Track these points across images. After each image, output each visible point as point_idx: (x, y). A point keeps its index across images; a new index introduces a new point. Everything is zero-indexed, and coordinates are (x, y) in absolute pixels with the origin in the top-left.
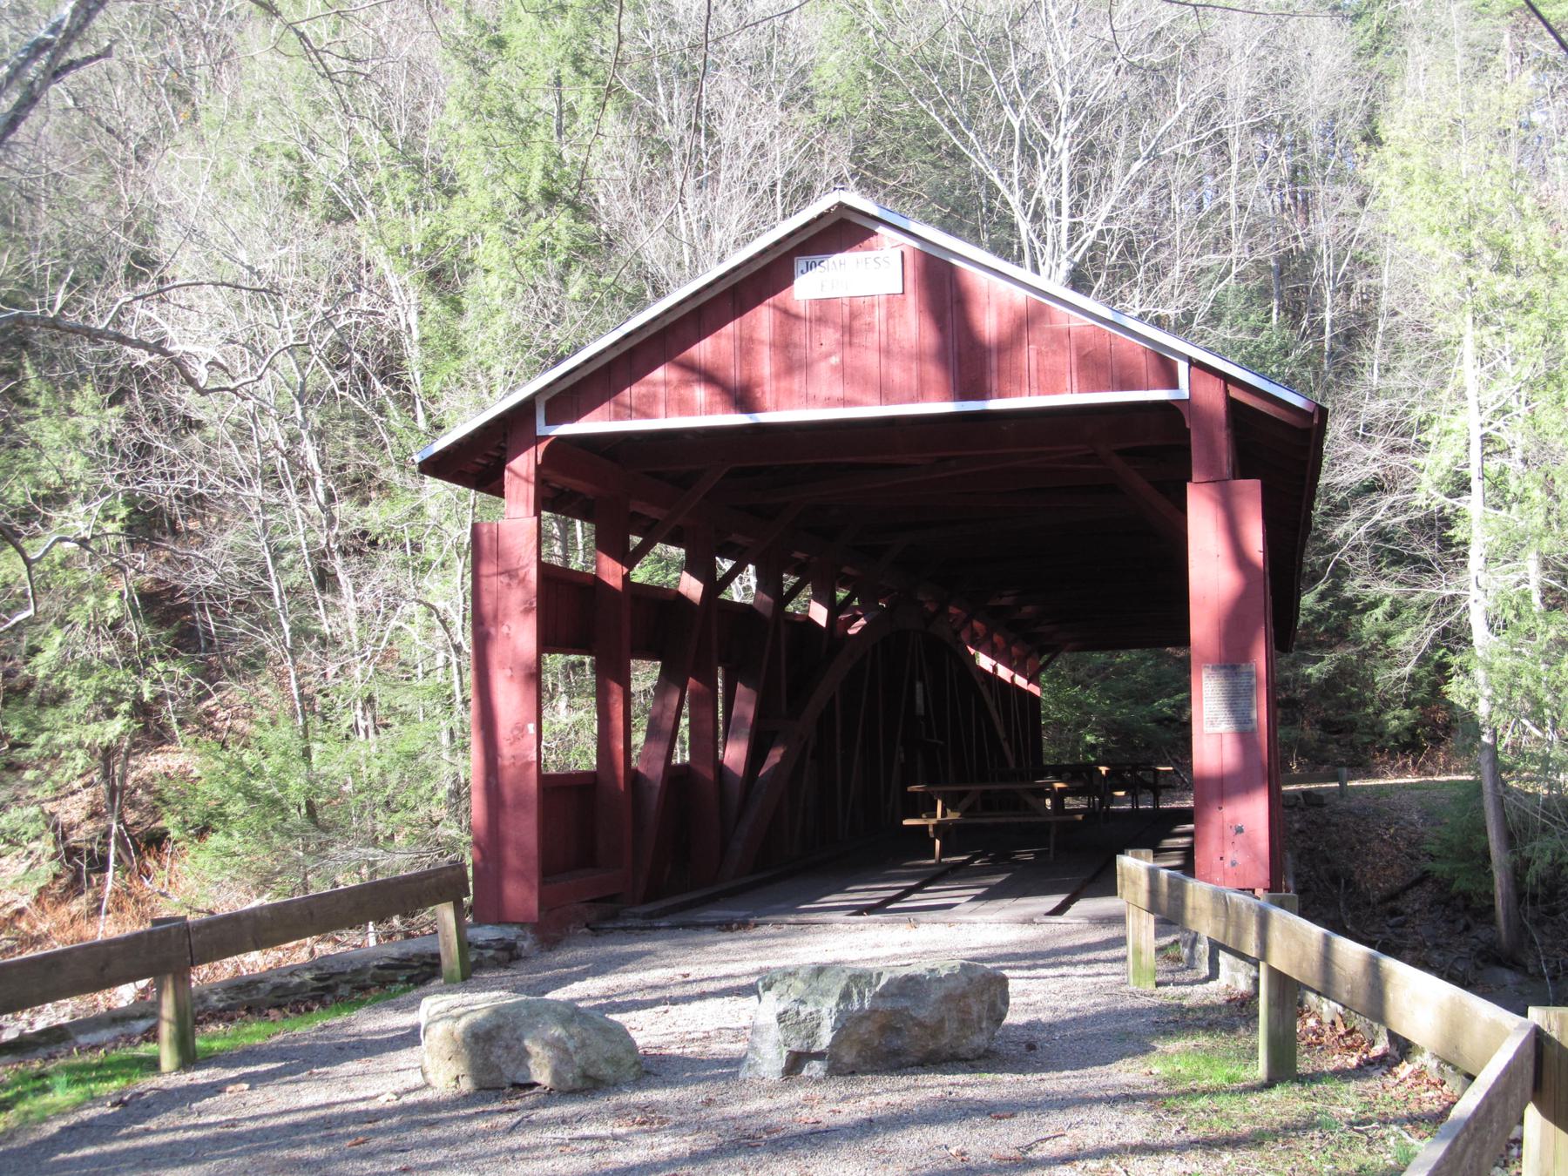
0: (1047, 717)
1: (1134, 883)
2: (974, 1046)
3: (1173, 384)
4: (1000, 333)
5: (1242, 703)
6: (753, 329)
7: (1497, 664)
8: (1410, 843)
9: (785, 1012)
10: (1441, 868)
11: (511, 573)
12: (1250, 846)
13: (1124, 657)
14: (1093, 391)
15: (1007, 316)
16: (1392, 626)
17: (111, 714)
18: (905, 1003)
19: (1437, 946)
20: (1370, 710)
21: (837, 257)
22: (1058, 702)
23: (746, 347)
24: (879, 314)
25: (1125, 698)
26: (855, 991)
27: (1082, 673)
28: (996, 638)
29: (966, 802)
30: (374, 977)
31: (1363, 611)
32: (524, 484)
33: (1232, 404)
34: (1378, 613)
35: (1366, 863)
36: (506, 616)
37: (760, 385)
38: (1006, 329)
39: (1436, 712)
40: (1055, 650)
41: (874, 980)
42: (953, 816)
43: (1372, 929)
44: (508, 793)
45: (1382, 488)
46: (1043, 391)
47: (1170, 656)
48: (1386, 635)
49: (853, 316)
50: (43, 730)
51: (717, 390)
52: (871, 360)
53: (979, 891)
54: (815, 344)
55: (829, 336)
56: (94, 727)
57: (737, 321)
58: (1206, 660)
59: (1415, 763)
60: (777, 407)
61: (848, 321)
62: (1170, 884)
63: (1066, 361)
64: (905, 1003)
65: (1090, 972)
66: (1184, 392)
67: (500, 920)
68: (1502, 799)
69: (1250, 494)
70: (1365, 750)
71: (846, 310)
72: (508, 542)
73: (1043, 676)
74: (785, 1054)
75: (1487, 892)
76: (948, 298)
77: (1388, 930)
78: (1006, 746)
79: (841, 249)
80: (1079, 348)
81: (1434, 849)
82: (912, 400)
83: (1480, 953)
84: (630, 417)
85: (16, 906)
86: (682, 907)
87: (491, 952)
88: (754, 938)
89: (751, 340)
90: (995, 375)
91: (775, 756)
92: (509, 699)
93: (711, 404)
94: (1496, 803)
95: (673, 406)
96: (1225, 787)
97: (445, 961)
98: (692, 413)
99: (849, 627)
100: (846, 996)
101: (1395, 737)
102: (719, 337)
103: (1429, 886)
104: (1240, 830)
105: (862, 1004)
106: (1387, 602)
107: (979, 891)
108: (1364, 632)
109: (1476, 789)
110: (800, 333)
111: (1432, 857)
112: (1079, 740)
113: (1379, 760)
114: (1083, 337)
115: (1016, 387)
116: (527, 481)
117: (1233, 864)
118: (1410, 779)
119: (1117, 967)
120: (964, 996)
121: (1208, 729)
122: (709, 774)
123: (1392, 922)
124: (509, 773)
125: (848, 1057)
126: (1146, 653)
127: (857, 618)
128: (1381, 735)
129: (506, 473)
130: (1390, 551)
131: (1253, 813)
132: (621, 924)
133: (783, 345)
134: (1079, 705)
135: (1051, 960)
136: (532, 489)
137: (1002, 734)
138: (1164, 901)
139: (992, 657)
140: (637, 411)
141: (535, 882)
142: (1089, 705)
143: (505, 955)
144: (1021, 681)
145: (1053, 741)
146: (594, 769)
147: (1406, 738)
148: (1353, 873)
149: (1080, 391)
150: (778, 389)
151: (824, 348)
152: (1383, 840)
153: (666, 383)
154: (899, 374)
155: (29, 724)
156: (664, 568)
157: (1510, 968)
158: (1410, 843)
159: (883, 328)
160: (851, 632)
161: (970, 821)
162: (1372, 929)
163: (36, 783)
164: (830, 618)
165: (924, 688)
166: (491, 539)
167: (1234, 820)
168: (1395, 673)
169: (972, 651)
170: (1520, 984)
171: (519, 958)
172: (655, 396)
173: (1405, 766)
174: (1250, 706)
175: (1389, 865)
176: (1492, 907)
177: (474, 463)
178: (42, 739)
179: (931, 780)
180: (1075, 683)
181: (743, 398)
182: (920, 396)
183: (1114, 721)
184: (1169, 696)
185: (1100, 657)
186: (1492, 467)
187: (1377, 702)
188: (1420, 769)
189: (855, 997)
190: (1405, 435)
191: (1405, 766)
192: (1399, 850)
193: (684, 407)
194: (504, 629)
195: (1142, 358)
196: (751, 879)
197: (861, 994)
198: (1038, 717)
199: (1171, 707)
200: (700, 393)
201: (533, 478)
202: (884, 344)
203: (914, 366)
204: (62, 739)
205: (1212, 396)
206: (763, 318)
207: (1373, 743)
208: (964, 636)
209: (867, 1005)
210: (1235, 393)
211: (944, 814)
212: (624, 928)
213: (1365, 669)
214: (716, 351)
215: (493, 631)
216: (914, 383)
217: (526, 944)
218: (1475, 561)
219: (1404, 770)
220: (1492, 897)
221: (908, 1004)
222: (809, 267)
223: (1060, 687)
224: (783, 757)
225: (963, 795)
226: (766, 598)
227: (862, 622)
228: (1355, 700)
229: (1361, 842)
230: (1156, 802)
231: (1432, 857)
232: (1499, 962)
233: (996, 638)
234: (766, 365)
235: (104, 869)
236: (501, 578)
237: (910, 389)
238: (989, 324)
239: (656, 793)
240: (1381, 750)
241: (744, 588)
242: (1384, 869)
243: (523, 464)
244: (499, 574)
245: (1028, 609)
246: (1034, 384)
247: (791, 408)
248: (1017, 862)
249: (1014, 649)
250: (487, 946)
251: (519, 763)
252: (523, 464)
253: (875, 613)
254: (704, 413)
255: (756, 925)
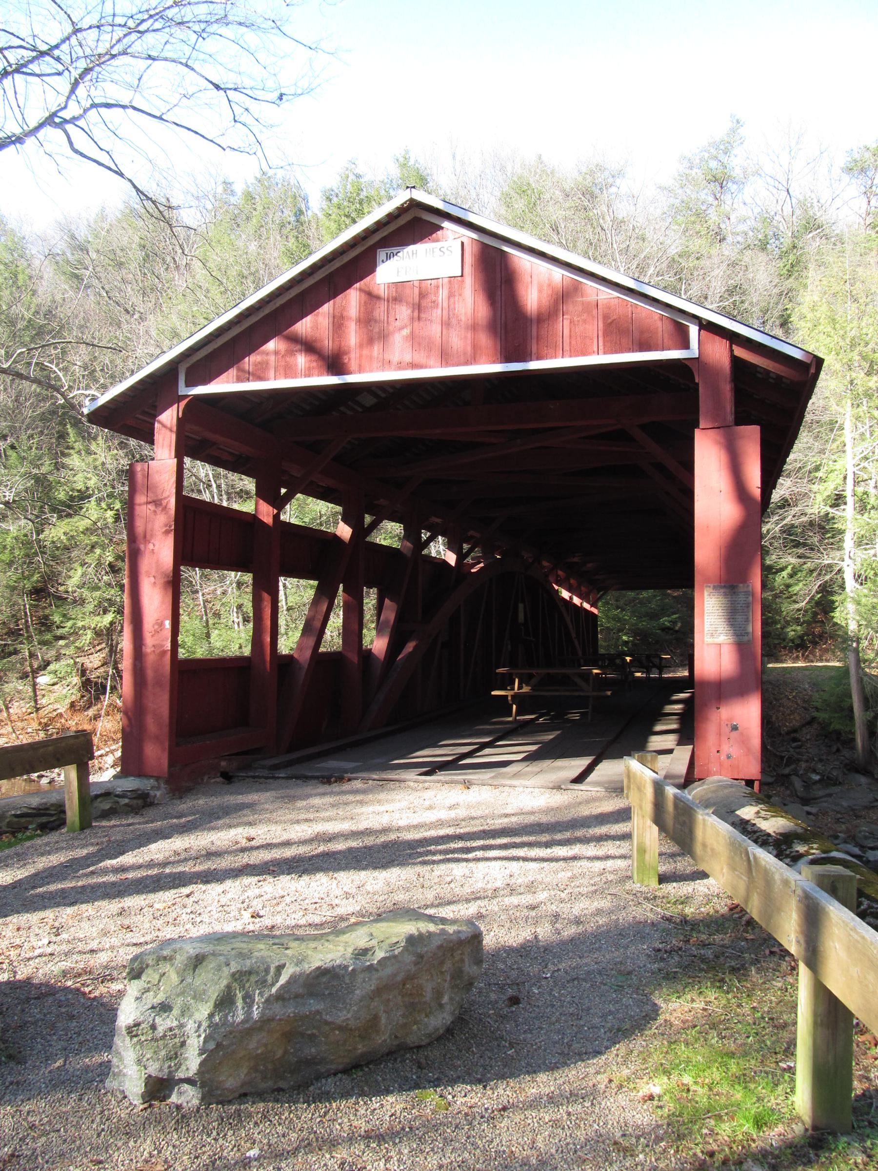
0: (602, 625)
1: (639, 789)
2: (431, 1028)
3: (685, 344)
4: (539, 307)
5: (740, 618)
6: (344, 308)
7: (864, 600)
8: (804, 701)
9: (137, 1025)
10: (823, 716)
11: (157, 503)
12: (744, 741)
13: (645, 594)
14: (616, 352)
15: (546, 292)
16: (791, 581)
17: (105, 611)
18: (314, 1005)
19: (821, 760)
20: (779, 626)
21: (411, 248)
22: (608, 617)
23: (338, 323)
24: (443, 294)
25: (645, 616)
26: (239, 995)
27: (621, 603)
28: (572, 581)
29: (534, 681)
30: (9, 824)
31: (776, 573)
32: (168, 433)
33: (736, 362)
34: (784, 574)
35: (779, 711)
36: (152, 535)
37: (347, 353)
38: (546, 302)
39: (814, 628)
40: (606, 589)
41: (269, 979)
42: (526, 689)
43: (782, 749)
44: (150, 674)
45: (789, 505)
46: (574, 353)
47: (669, 595)
48: (788, 586)
49: (422, 295)
50: (70, 619)
51: (314, 357)
52: (435, 330)
53: (534, 748)
54: (391, 319)
55: (403, 312)
56: (98, 618)
57: (331, 302)
58: (707, 581)
59: (803, 655)
60: (360, 370)
61: (419, 298)
62: (676, 806)
63: (594, 328)
64: (314, 1005)
65: (601, 852)
66: (694, 351)
67: (140, 773)
68: (862, 679)
69: (751, 440)
70: (775, 647)
71: (417, 291)
72: (156, 478)
73: (600, 604)
74: (144, 1077)
75: (850, 731)
76: (498, 276)
77: (791, 750)
78: (576, 642)
79: (414, 242)
80: (605, 317)
81: (818, 705)
82: (467, 363)
83: (846, 765)
84: (248, 380)
85: (59, 711)
86: (299, 761)
87: (126, 801)
88: (338, 794)
89: (342, 317)
90: (534, 341)
91: (410, 647)
92: (154, 601)
93: (309, 369)
94: (858, 681)
95: (281, 371)
96: (724, 690)
97: (69, 814)
98: (294, 376)
99: (473, 568)
100: (225, 1002)
101: (792, 641)
102: (317, 315)
103: (815, 726)
104: (735, 728)
105: (248, 1013)
106: (790, 568)
107: (534, 748)
108: (776, 584)
109: (844, 672)
110: (380, 311)
111: (817, 709)
112: (619, 638)
113: (783, 653)
114: (609, 308)
115: (551, 351)
116: (171, 431)
117: (729, 757)
118: (800, 664)
119: (622, 848)
120: (410, 977)
121: (708, 639)
122: (354, 658)
123: (794, 745)
124: (151, 659)
125: (231, 1080)
126: (657, 592)
127: (479, 563)
128: (784, 640)
129: (156, 425)
130: (794, 538)
131: (748, 713)
132: (251, 774)
133: (367, 320)
134: (619, 620)
135: (568, 835)
136: (174, 436)
137: (574, 635)
138: (670, 821)
139: (569, 592)
140: (253, 375)
141: (167, 744)
142: (625, 620)
143: (140, 802)
144: (586, 606)
145: (605, 640)
146: (340, 650)
147: (798, 642)
148: (771, 717)
149: (605, 353)
150: (361, 356)
151: (398, 323)
152: (789, 699)
153: (276, 353)
154: (458, 341)
155: (64, 616)
156: (309, 511)
157: (863, 774)
158: (804, 701)
159: (445, 305)
160: (473, 571)
161: (537, 693)
162: (782, 749)
163: (67, 646)
164: (458, 561)
165: (525, 608)
166: (143, 475)
167: (730, 719)
168: (797, 606)
169: (556, 587)
170: (870, 784)
171: (152, 804)
172: (267, 363)
173: (797, 657)
174: (747, 620)
175: (792, 712)
176: (853, 740)
177: (128, 418)
178: (69, 624)
179: (512, 664)
180: (618, 608)
181: (335, 363)
182: (473, 360)
183: (638, 629)
184: (669, 616)
185: (631, 594)
186: (860, 490)
187: (782, 622)
188: (806, 659)
189: (240, 1003)
190: (812, 473)
191: (797, 657)
192: (797, 704)
193: (289, 371)
194: (151, 546)
195: (659, 324)
196: (389, 729)
197: (248, 999)
198: (596, 626)
199: (670, 622)
200: (302, 360)
201: (175, 429)
202: (445, 318)
203: (469, 335)
204: (80, 624)
205: (719, 353)
206: (352, 300)
207: (780, 644)
208: (551, 579)
209: (256, 1013)
210: (739, 352)
211: (520, 688)
212: (254, 777)
213: (776, 604)
214: (316, 326)
215: (142, 547)
216: (469, 349)
217: (158, 793)
218: (848, 543)
219: (796, 659)
220: (854, 733)
221: (320, 1006)
222: (388, 257)
223: (609, 610)
224: (415, 648)
225: (531, 676)
226: (409, 544)
227: (482, 565)
228: (770, 621)
229: (776, 700)
230: (660, 673)
231: (817, 709)
232: (857, 771)
233: (572, 581)
234: (353, 337)
235: (104, 693)
236: (149, 506)
237: (465, 354)
238: (532, 298)
239: (302, 676)
240: (785, 648)
241: (389, 534)
242: (789, 715)
243: (169, 417)
244: (148, 503)
245: (590, 565)
246: (567, 348)
247: (371, 371)
248: (569, 721)
249: (583, 588)
250: (123, 796)
251: (158, 651)
252: (169, 417)
253: (491, 560)
254: (307, 376)
255: (349, 780)
